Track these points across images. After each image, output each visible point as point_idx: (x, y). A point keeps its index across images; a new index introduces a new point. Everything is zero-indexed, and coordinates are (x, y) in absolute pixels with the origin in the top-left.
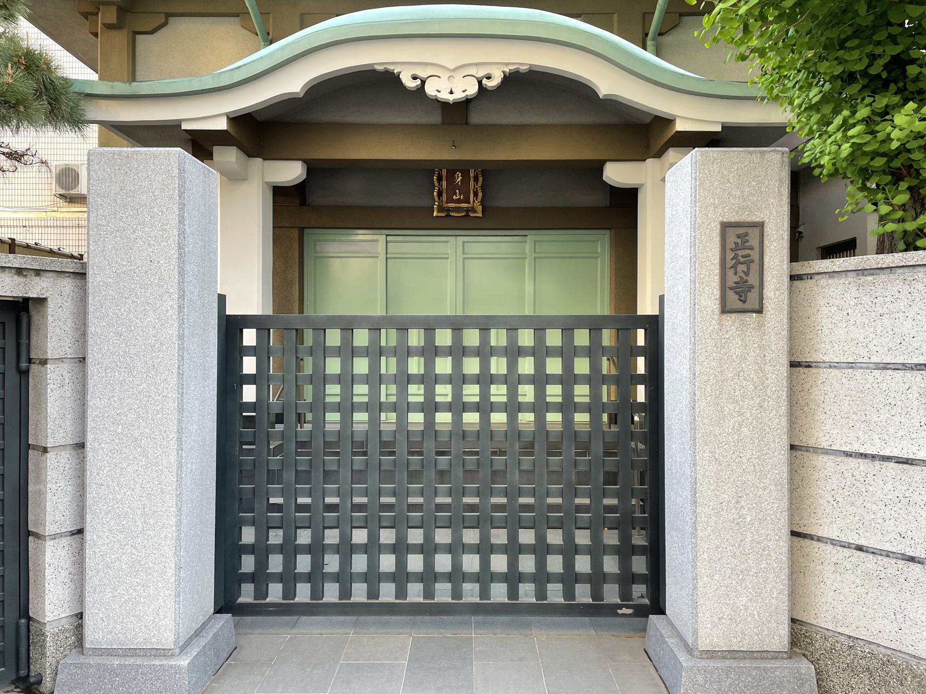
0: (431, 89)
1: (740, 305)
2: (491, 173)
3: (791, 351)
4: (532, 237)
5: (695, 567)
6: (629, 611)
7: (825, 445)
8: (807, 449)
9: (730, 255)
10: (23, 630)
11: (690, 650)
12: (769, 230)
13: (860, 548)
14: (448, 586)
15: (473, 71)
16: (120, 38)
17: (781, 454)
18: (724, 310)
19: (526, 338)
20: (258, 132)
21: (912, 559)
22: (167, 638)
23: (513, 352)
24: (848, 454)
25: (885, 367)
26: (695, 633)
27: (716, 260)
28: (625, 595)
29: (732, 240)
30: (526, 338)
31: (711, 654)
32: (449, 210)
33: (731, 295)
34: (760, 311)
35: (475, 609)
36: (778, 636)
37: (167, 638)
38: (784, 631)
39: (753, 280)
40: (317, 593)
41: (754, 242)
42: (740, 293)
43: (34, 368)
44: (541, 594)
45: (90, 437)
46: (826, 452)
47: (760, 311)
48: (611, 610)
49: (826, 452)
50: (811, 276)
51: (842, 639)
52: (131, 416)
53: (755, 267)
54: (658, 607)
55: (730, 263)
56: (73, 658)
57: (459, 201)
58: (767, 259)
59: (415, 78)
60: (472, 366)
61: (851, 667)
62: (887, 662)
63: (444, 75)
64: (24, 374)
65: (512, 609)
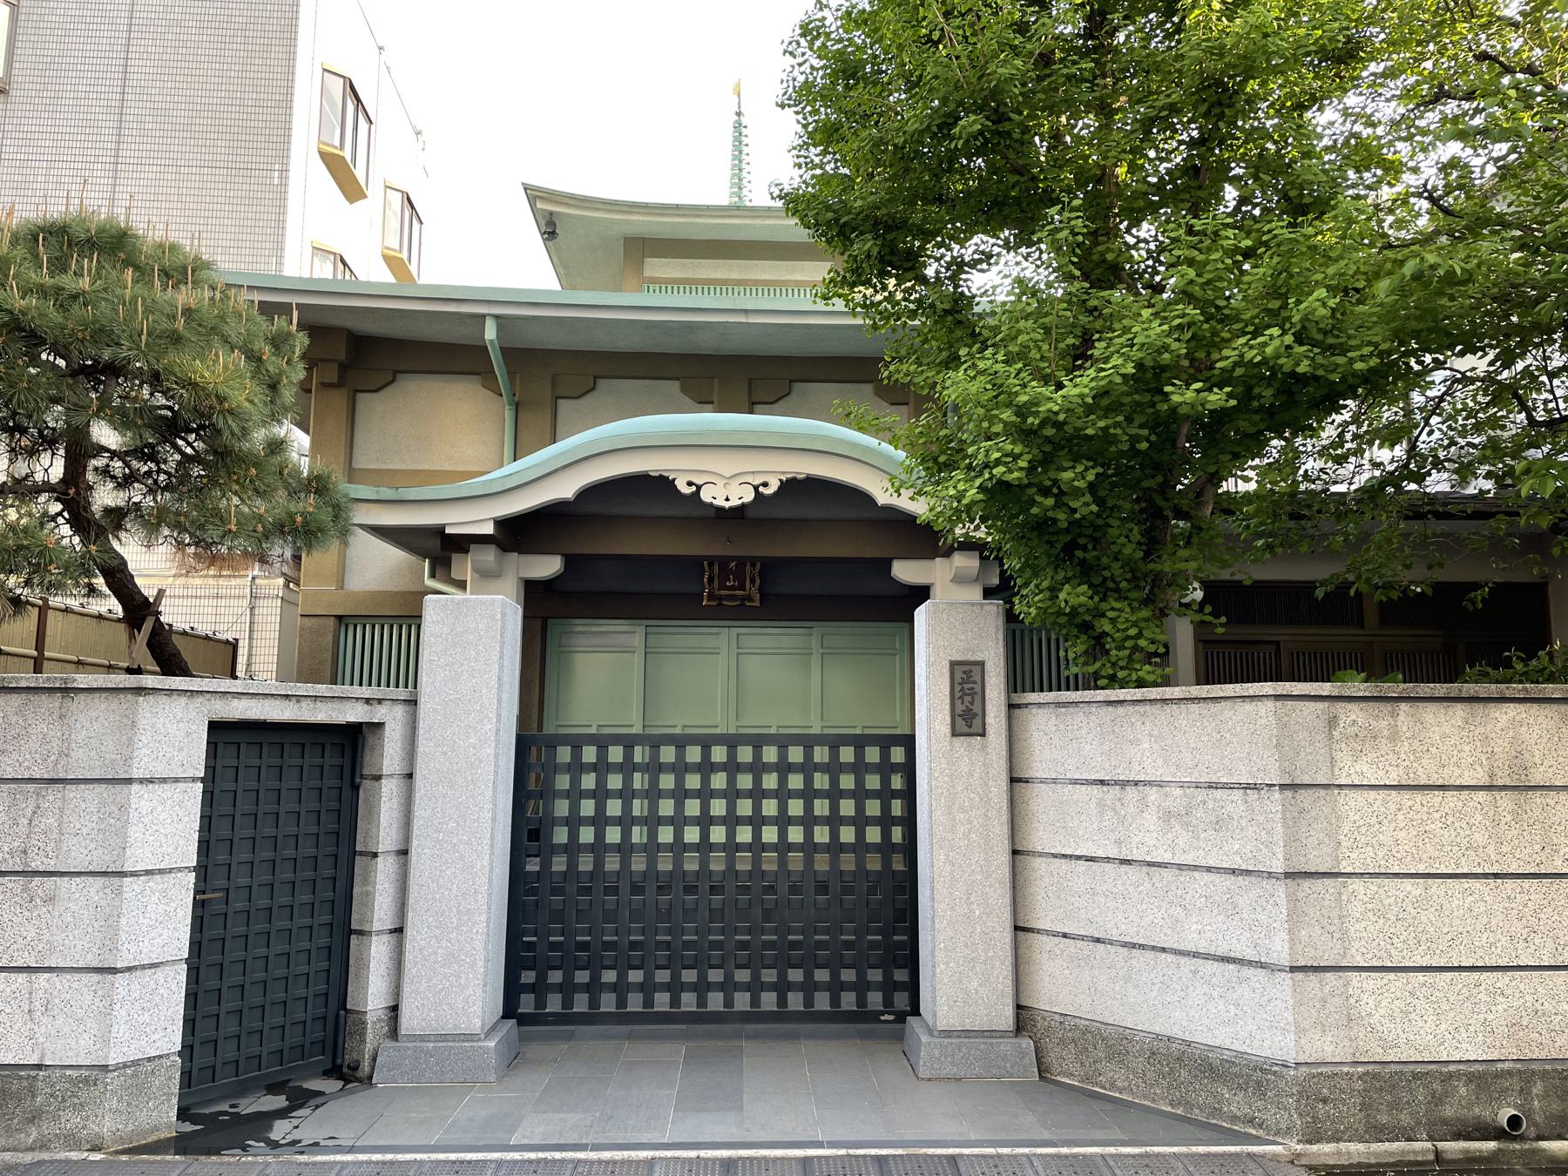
0: (706, 496)
1: (966, 730)
2: (769, 568)
3: (1011, 769)
4: (819, 628)
5: (933, 957)
6: (891, 1018)
7: (1039, 849)
8: (1028, 853)
9: (958, 688)
10: (342, 1020)
11: (930, 1032)
12: (989, 667)
13: (1065, 936)
14: (720, 996)
15: (749, 479)
16: (339, 398)
17: (1004, 858)
18: (954, 734)
19: (796, 754)
20: (518, 533)
21: (1098, 940)
22: (476, 1024)
23: (784, 768)
24: (1055, 856)
25: (1075, 782)
26: (935, 1015)
27: (947, 692)
28: (888, 1002)
29: (959, 675)
30: (821, 754)
31: (948, 1034)
32: (721, 598)
33: (959, 721)
34: (983, 735)
35: (745, 1017)
36: (1005, 1018)
37: (476, 1024)
38: (1009, 1012)
39: (976, 708)
40: (594, 1003)
41: (977, 678)
42: (966, 719)
43: (366, 784)
44: (809, 1002)
45: (415, 843)
46: (1041, 855)
47: (983, 735)
48: (874, 1017)
49: (1041, 855)
50: (1026, 705)
51: (1057, 1017)
52: (452, 825)
53: (978, 698)
54: (915, 1011)
55: (958, 695)
56: (389, 1044)
57: (733, 588)
58: (987, 692)
59: (690, 484)
60: (745, 781)
61: (1062, 1042)
62: (1087, 1030)
63: (720, 483)
64: (356, 788)
65: (782, 1016)
